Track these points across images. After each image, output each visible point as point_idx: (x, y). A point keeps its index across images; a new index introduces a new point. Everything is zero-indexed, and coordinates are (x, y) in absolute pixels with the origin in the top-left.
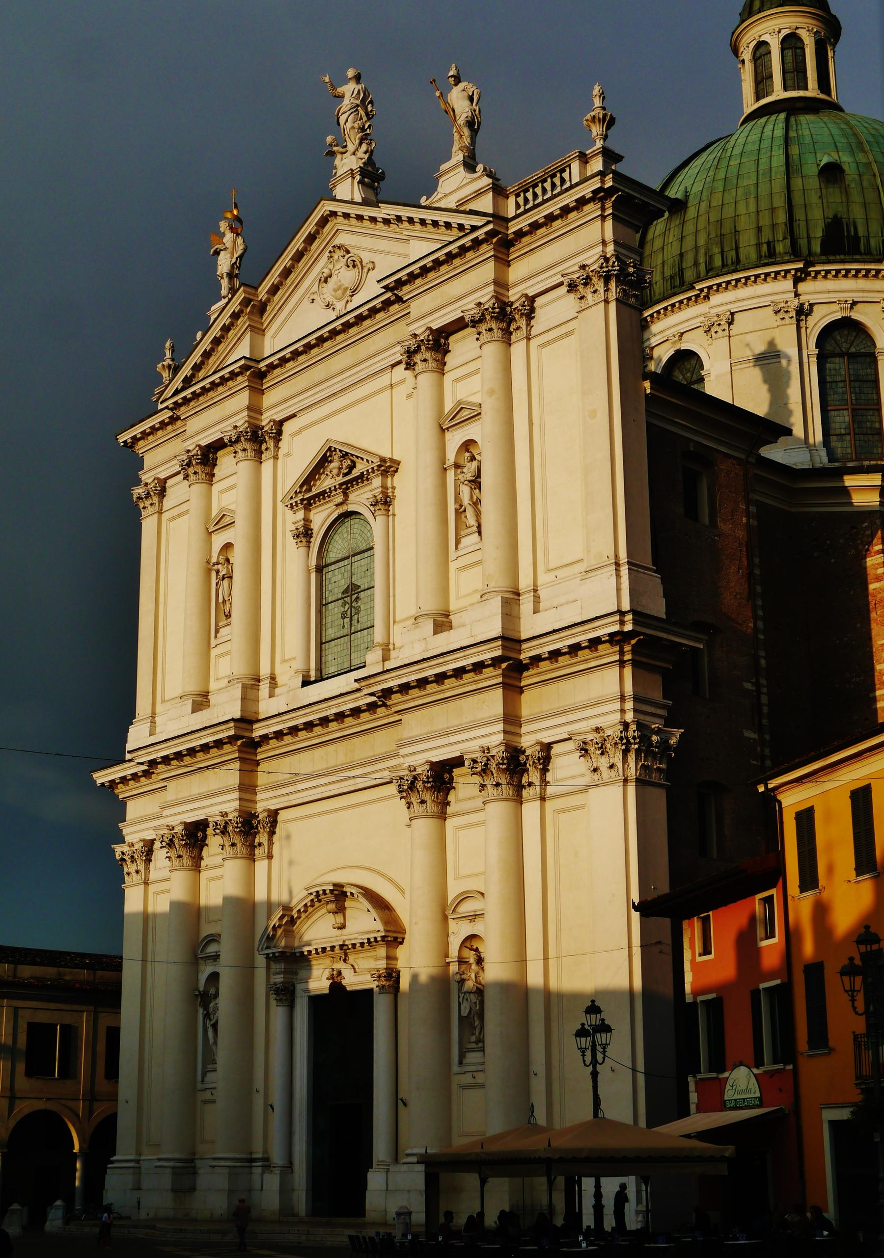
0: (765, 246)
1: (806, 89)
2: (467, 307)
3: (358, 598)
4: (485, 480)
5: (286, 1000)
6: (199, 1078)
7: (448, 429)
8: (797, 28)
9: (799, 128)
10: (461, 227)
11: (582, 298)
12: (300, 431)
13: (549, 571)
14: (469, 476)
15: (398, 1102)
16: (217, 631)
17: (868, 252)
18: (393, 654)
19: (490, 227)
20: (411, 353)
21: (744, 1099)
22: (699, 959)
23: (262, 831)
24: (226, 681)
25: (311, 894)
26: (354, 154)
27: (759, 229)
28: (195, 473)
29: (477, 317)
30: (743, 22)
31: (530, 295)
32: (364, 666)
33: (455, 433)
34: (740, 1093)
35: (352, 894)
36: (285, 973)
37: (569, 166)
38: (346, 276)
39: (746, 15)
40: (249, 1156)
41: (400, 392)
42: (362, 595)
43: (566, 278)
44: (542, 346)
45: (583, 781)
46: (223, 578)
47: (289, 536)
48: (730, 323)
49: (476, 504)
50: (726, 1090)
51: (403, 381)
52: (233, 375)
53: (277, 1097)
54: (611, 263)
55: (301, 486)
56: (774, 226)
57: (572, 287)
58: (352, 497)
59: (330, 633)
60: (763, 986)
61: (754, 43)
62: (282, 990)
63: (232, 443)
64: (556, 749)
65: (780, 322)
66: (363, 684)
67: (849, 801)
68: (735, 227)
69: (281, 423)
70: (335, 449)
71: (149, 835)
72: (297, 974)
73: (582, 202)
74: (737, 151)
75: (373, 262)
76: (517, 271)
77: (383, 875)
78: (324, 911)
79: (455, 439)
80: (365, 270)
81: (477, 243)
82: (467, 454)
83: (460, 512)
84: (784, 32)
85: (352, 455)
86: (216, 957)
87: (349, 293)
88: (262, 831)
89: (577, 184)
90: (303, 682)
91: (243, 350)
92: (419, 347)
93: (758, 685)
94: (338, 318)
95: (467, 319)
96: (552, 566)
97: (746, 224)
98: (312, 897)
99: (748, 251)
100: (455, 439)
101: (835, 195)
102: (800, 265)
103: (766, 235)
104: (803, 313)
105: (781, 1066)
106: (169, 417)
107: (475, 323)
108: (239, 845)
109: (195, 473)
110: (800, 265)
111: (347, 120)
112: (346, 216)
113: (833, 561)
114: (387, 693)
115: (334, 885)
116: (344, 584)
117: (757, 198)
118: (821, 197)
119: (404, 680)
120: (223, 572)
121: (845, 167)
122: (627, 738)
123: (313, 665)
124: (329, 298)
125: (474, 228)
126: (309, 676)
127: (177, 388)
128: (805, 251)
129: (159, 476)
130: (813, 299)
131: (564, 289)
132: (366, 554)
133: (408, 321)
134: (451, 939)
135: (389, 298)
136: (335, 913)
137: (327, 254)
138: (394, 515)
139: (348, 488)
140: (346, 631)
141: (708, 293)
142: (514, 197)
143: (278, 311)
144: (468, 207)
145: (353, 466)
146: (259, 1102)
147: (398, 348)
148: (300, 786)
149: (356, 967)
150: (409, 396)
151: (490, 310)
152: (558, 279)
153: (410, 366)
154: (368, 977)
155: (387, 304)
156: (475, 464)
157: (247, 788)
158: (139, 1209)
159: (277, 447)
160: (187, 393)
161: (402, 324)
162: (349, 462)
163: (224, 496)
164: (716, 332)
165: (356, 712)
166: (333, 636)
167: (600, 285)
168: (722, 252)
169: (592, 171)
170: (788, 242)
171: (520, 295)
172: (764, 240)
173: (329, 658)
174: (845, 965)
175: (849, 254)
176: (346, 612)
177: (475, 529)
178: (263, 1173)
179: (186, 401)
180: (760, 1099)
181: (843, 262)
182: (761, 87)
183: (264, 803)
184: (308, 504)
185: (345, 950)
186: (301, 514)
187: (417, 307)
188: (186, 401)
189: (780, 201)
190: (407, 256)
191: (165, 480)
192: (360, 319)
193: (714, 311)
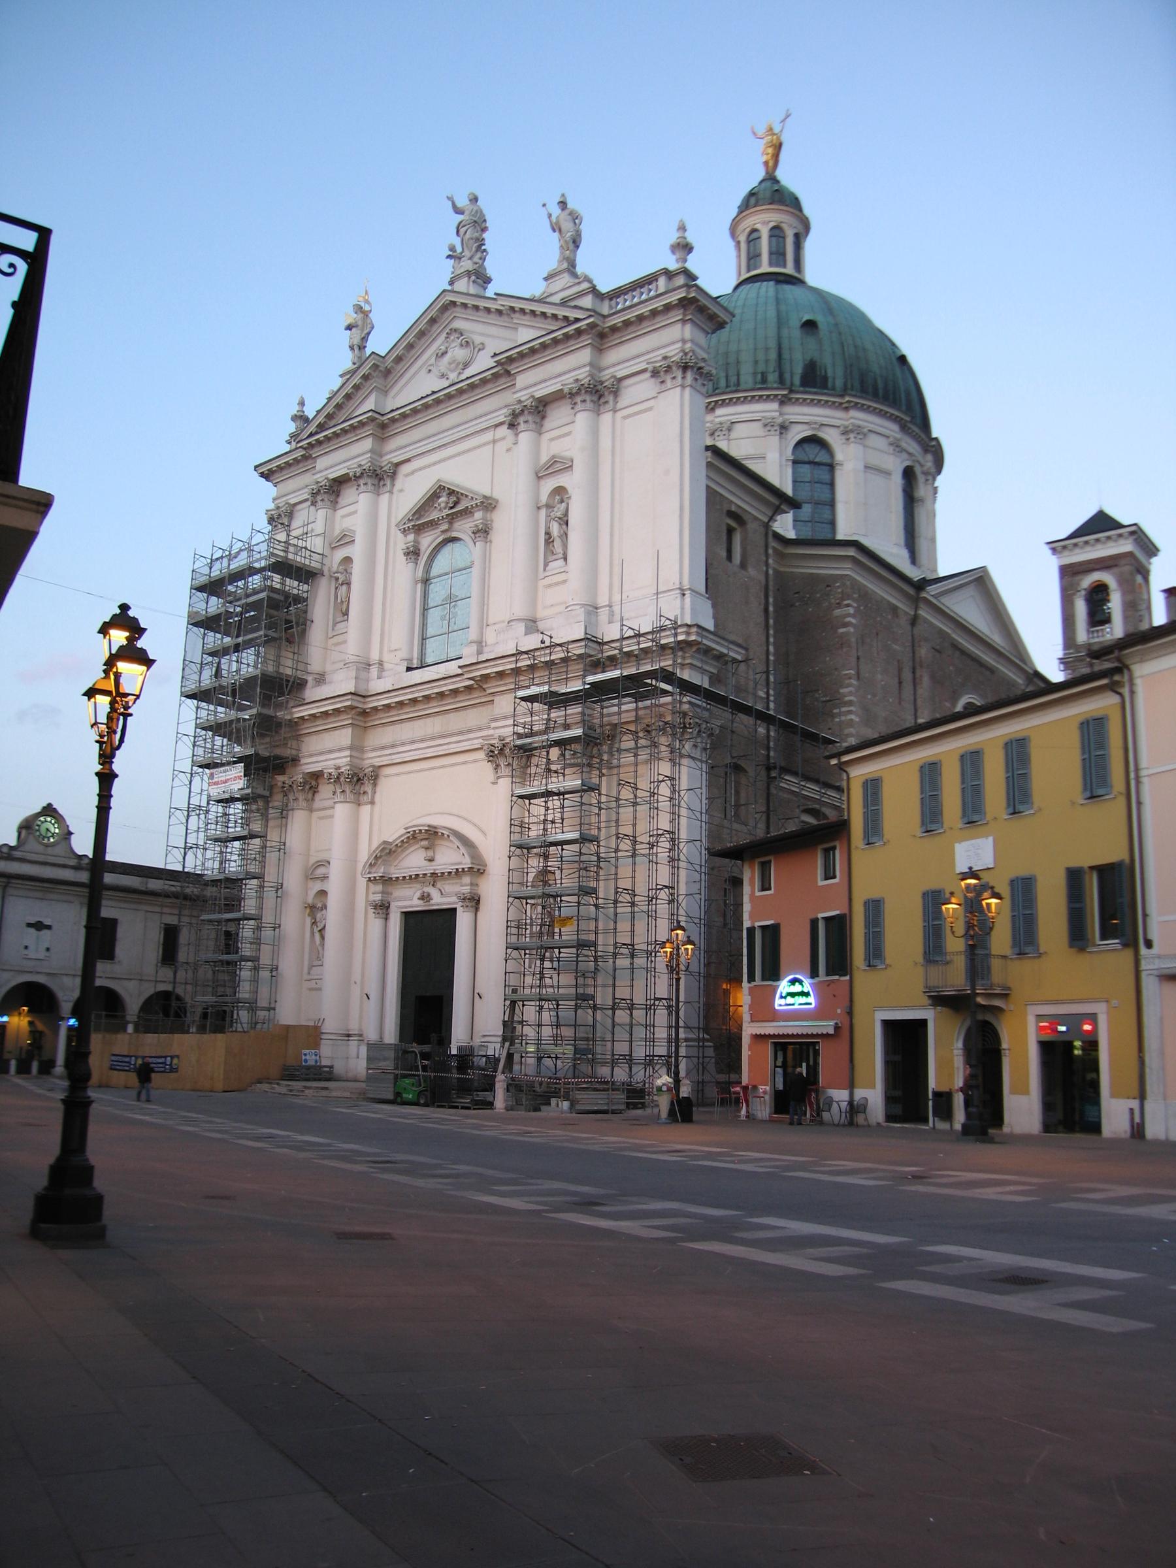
1: (785, 266)
2: (567, 382)
4: (573, 519)
5: (472, 907)
7: (542, 477)
8: (781, 222)
10: (566, 318)
11: (662, 382)
12: (413, 473)
13: (392, 651)
14: (559, 514)
15: (475, 995)
17: (834, 389)
18: (486, 649)
19: (591, 320)
20: (314, 494)
22: (758, 894)
23: (367, 782)
24: (342, 663)
25: (409, 832)
26: (470, 258)
27: (756, 362)
28: (322, 500)
29: (574, 391)
30: (742, 212)
31: (618, 377)
33: (548, 480)
36: (383, 893)
38: (458, 353)
39: (743, 208)
40: (586, 1036)
41: (501, 447)
44: (625, 418)
46: (342, 584)
47: (401, 553)
48: (729, 430)
49: (565, 536)
51: (503, 438)
52: (362, 424)
53: (373, 989)
54: (688, 357)
55: (414, 515)
56: (767, 361)
57: (655, 373)
58: (457, 525)
59: (430, 631)
60: (820, 915)
61: (748, 229)
62: (380, 906)
63: (357, 478)
65: (767, 433)
66: (465, 670)
70: (444, 487)
72: (391, 894)
73: (668, 308)
74: (740, 303)
76: (612, 356)
77: (469, 821)
78: (417, 846)
80: (476, 350)
81: (579, 332)
82: (558, 497)
83: (549, 540)
84: (772, 224)
85: (458, 492)
86: (325, 878)
87: (461, 366)
88: (367, 782)
89: (661, 294)
90: (407, 668)
91: (370, 404)
92: (523, 411)
93: (768, 693)
94: (450, 386)
95: (565, 391)
96: (393, 648)
97: (746, 357)
98: (409, 835)
99: (747, 379)
101: (811, 343)
102: (785, 392)
103: (761, 367)
104: (784, 428)
106: (302, 456)
107: (572, 395)
108: (348, 791)
109: (322, 500)
110: (785, 392)
111: (466, 232)
112: (465, 306)
114: (486, 677)
115: (429, 826)
117: (755, 339)
118: (802, 344)
119: (500, 669)
120: (342, 578)
121: (820, 326)
122: (684, 723)
123: (415, 655)
124: (443, 369)
125: (577, 320)
126: (412, 664)
128: (788, 383)
129: (290, 501)
130: (793, 418)
131: (648, 375)
132: (464, 572)
133: (314, 472)
134: (309, 892)
135: (498, 372)
136: (427, 848)
137: (444, 335)
138: (491, 541)
139: (453, 519)
140: (445, 630)
141: (715, 405)
144: (573, 304)
145: (456, 503)
146: (356, 992)
147: (505, 411)
148: (401, 749)
149: (443, 891)
150: (509, 450)
151: (586, 385)
153: (512, 426)
154: (454, 899)
155: (496, 376)
156: (564, 505)
157: (357, 748)
159: (393, 485)
160: (320, 436)
161: (308, 475)
162: (455, 499)
163: (346, 519)
164: (718, 436)
165: (455, 692)
166: (433, 634)
167: (679, 374)
168: (727, 377)
170: (777, 374)
171: (610, 376)
173: (429, 650)
175: (819, 388)
179: (319, 442)
181: (815, 393)
183: (372, 759)
184: (419, 529)
185: (435, 878)
187: (521, 380)
188: (319, 442)
189: (772, 344)
190: (517, 341)
192: (472, 387)
193: (717, 420)
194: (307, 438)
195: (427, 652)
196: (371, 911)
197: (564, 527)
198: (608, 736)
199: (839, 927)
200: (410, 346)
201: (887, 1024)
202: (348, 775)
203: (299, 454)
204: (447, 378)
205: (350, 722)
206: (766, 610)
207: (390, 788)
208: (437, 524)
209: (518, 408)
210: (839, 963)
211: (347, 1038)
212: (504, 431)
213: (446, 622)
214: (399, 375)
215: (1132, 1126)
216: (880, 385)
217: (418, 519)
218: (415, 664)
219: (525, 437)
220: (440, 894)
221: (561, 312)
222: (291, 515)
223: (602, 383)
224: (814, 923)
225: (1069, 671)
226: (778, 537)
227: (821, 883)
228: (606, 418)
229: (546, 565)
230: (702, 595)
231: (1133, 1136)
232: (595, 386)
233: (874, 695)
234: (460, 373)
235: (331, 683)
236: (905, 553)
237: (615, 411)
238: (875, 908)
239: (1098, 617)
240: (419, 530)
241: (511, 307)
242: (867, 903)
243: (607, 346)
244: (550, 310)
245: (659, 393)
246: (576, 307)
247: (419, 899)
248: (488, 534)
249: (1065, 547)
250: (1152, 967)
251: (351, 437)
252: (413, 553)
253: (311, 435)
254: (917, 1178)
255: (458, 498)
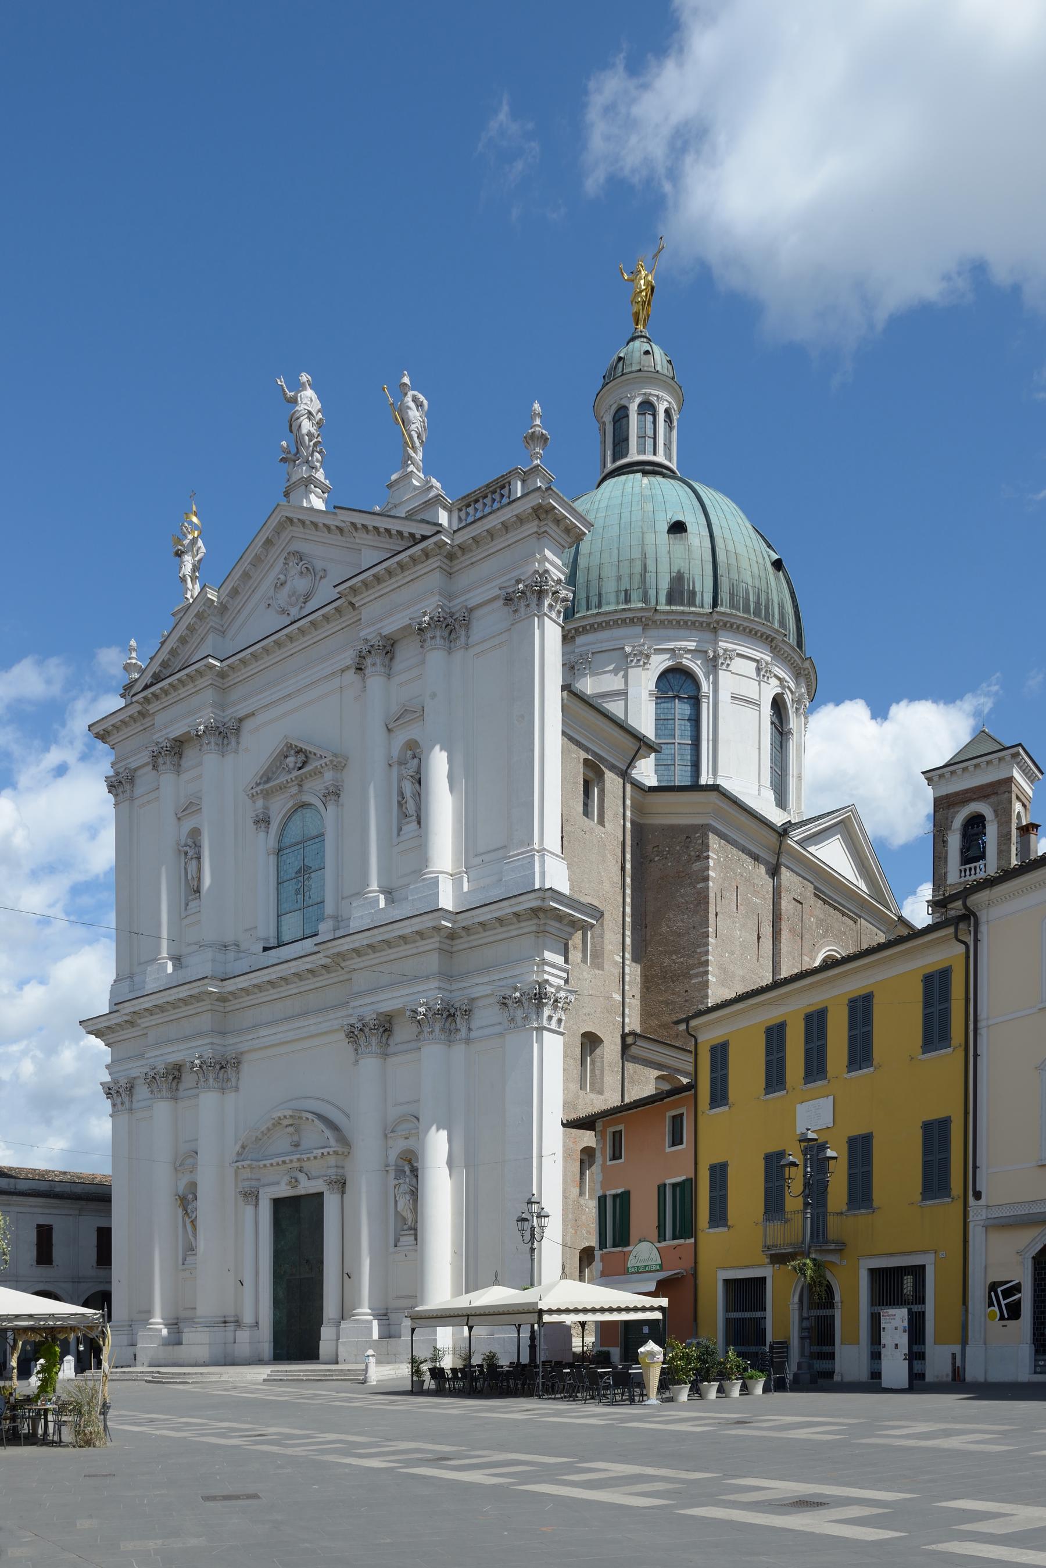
0: (623, 593)
3: (309, 877)
6: (180, 1262)
9: (653, 487)
10: (412, 535)
16: (187, 905)
20: (155, 757)
21: (645, 1266)
31: (469, 606)
32: (317, 935)
34: (641, 1261)
35: (307, 1119)
37: (509, 483)
38: (302, 584)
42: (313, 875)
43: (503, 591)
45: (497, 1029)
50: (630, 1259)
56: (631, 576)
57: (508, 600)
59: (286, 907)
60: (669, 1181)
64: (480, 1003)
67: (764, 1036)
68: (600, 574)
69: (241, 720)
71: (134, 1073)
73: (520, 520)
74: (603, 504)
75: (325, 570)
79: (401, 738)
80: (318, 578)
87: (302, 600)
93: (623, 957)
100: (401, 738)
103: (625, 585)
105: (681, 1241)
113: (669, 864)
116: (297, 865)
125: (424, 538)
127: (147, 684)
132: (317, 840)
137: (282, 560)
138: (342, 805)
142: (457, 511)
143: (237, 614)
145: (304, 763)
149: (309, 1175)
152: (498, 592)
153: (359, 669)
156: (416, 761)
158: (135, 1359)
159: (238, 743)
164: (578, 670)
166: (287, 910)
169: (529, 489)
172: (623, 588)
173: (285, 928)
174: (601, 1182)
176: (299, 889)
177: (414, 818)
178: (235, 1331)
180: (661, 1265)
182: (617, 448)
184: (267, 795)
186: (260, 803)
187: (160, 719)
191: (135, 770)
194: (142, 691)
195: (283, 930)
196: (241, 1199)
197: (417, 785)
198: (466, 1011)
199: (685, 1190)
200: (246, 576)
201: (727, 1282)
202: (211, 1063)
203: (135, 709)
204: (288, 614)
205: (209, 1007)
206: (623, 869)
207: (249, 1074)
208: (286, 787)
209: (365, 648)
210: (685, 1227)
211: (224, 1325)
212: (351, 676)
213: (300, 896)
214: (236, 612)
215: (954, 1371)
216: (752, 598)
217: (266, 782)
218: (273, 942)
219: (375, 681)
220: (307, 1178)
221: (408, 528)
222: (132, 780)
223: (452, 615)
224: (662, 1188)
225: (938, 915)
226: (637, 786)
227: (668, 1150)
228: (458, 655)
229: (400, 829)
230: (557, 856)
231: (954, 1379)
232: (445, 619)
233: (732, 953)
234: (301, 608)
235: (187, 967)
236: (770, 795)
237: (467, 647)
238: (719, 1173)
239: (972, 852)
240: (268, 794)
241: (352, 523)
242: (713, 1168)
243: (458, 568)
244: (394, 526)
245: (513, 624)
246: (423, 521)
247: (287, 1185)
248: (339, 797)
249: (941, 776)
250: (979, 1218)
251: (190, 688)
252: (263, 821)
253: (146, 687)
254: (740, 1422)
255: (306, 757)
